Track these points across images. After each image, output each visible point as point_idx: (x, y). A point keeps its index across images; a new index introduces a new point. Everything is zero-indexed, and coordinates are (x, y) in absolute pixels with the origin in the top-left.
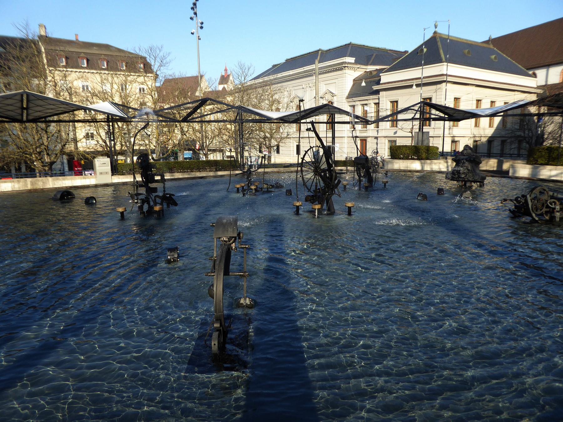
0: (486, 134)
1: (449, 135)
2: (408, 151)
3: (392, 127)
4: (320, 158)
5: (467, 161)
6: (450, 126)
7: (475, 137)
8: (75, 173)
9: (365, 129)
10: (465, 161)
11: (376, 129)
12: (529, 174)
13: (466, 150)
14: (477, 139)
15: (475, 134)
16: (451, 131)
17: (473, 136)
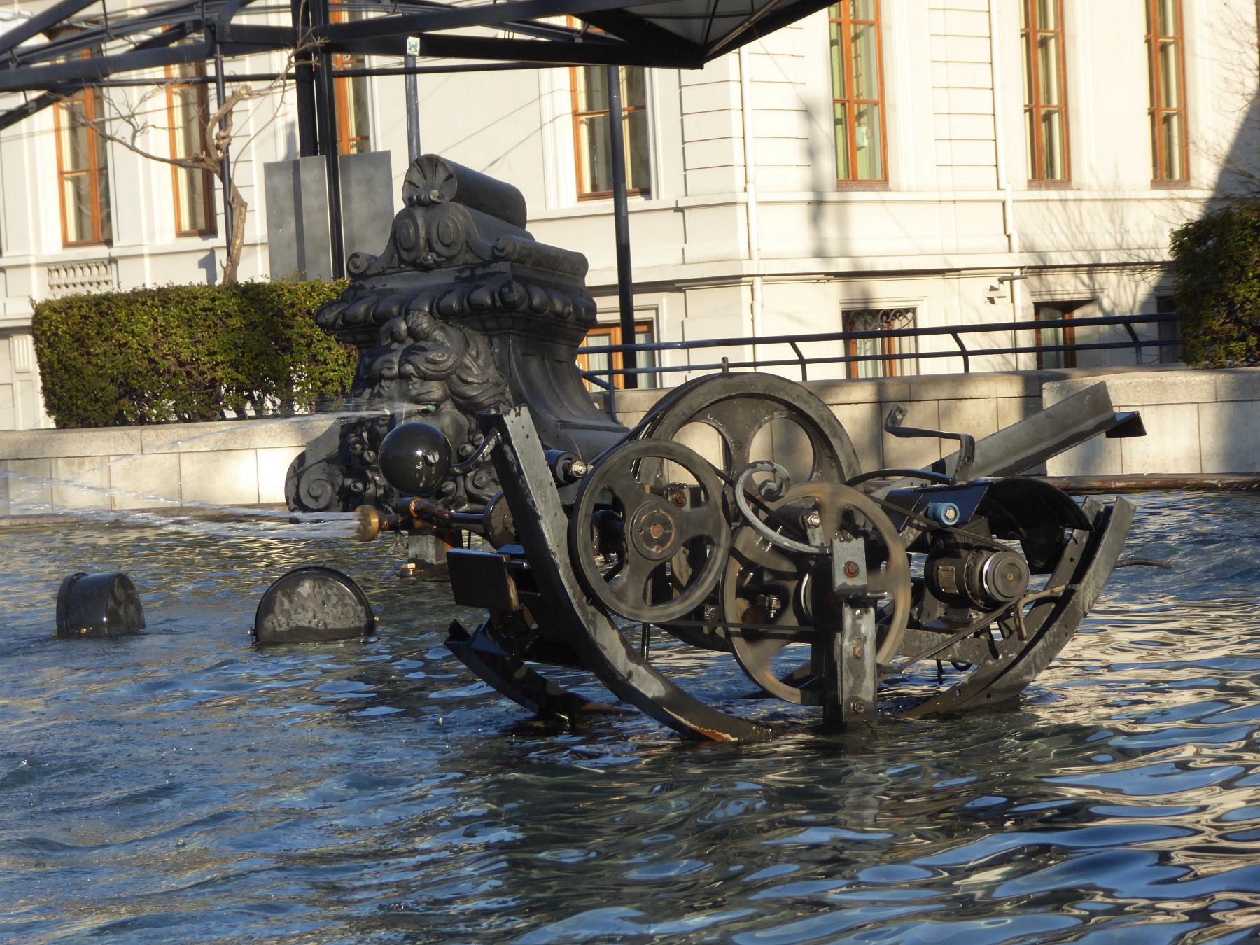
0: (1135, 238)
1: (816, 266)
2: (179, 335)
3: (82, 242)
4: (1031, 606)
5: (442, 315)
6: (817, 189)
7: (1040, 269)
8: (468, 706)
9: (101, 252)
10: (424, 323)
11: (197, 242)
12: (1210, 442)
13: (429, 205)
14: (1066, 287)
15: (1043, 242)
16: (830, 230)
17: (1029, 261)
